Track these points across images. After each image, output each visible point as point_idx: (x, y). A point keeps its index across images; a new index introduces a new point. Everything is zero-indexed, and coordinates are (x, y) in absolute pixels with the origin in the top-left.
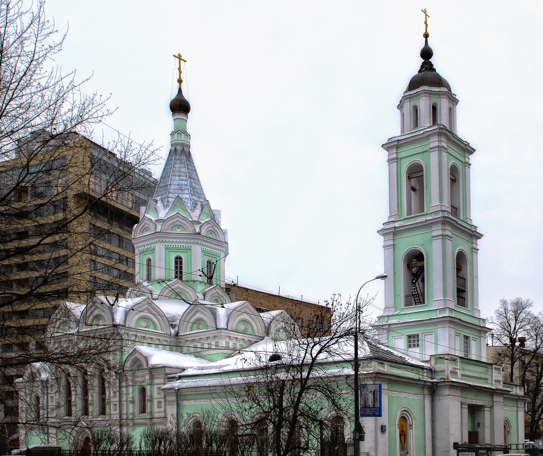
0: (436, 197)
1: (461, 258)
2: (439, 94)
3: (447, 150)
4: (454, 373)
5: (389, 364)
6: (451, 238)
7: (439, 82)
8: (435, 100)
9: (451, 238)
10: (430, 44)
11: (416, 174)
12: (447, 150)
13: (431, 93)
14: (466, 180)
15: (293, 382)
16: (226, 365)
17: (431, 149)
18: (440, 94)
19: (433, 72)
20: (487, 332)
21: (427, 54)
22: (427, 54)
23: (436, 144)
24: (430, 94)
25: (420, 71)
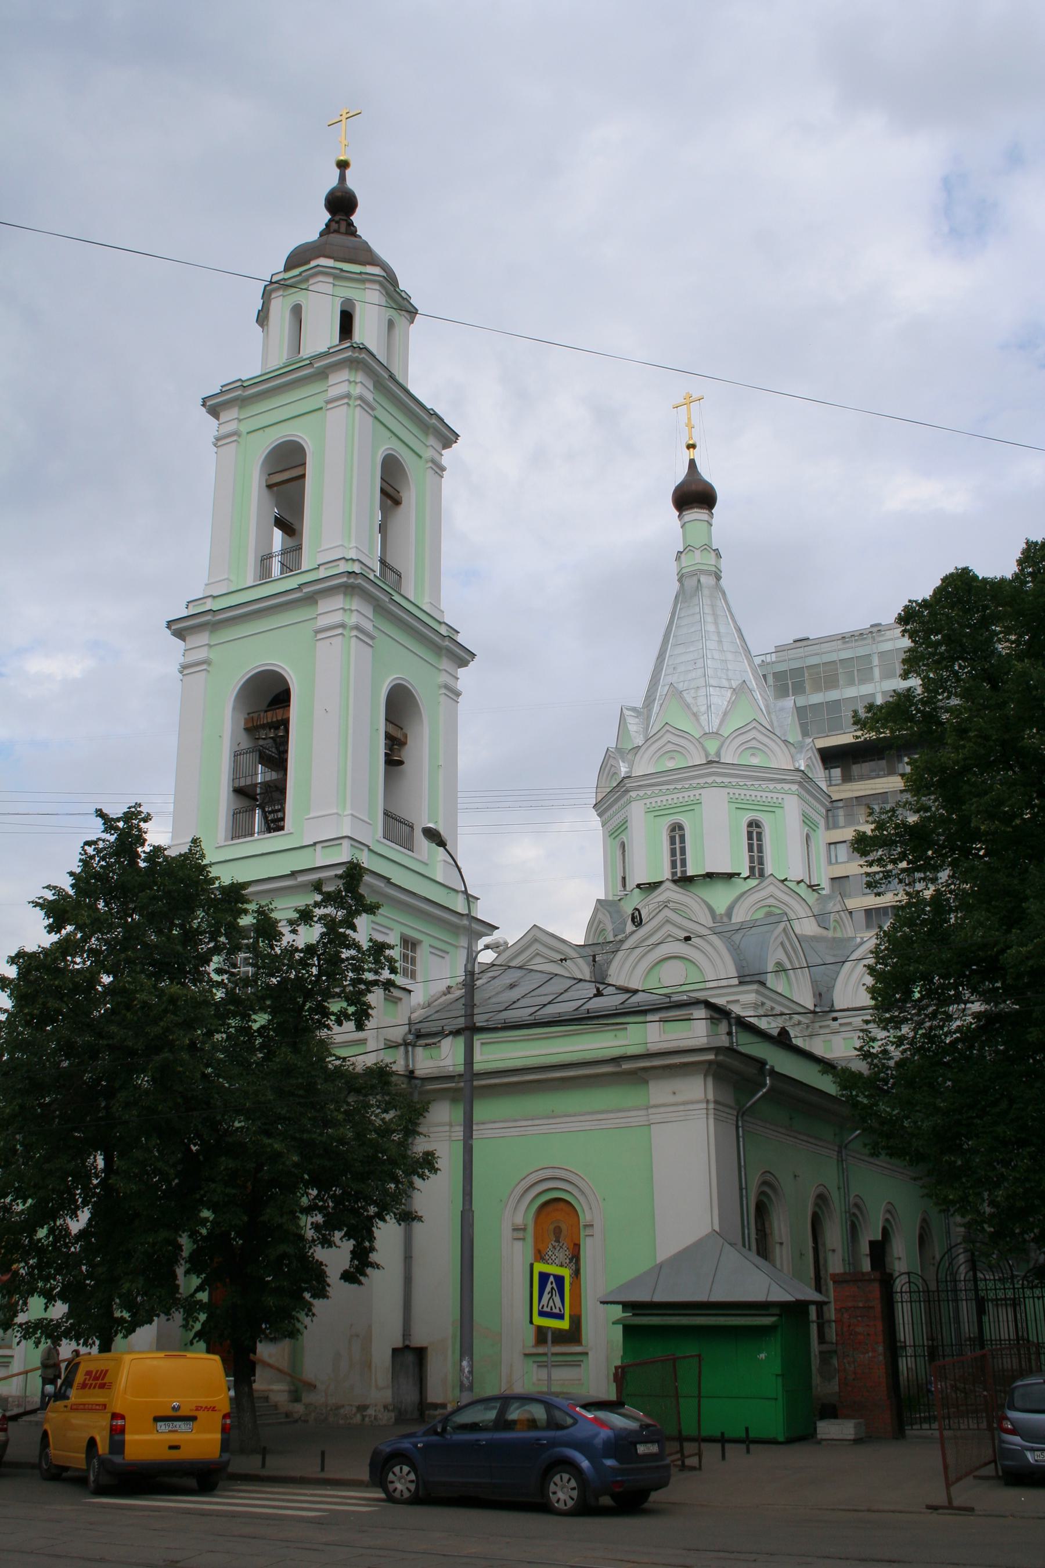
0: (338, 527)
1: (400, 706)
2: (362, 279)
3: (373, 409)
4: (769, 1023)
5: (656, 1017)
6: (372, 638)
7: (365, 255)
8: (348, 291)
9: (372, 638)
10: (351, 183)
11: (286, 478)
12: (373, 409)
13: (339, 276)
14: (528, 1040)
15: (409, 1044)
16: (797, 979)
17: (328, 402)
18: (363, 281)
19: (353, 239)
20: (481, 935)
21: (341, 204)
22: (341, 204)
23: (343, 389)
24: (336, 277)
25: (322, 234)
